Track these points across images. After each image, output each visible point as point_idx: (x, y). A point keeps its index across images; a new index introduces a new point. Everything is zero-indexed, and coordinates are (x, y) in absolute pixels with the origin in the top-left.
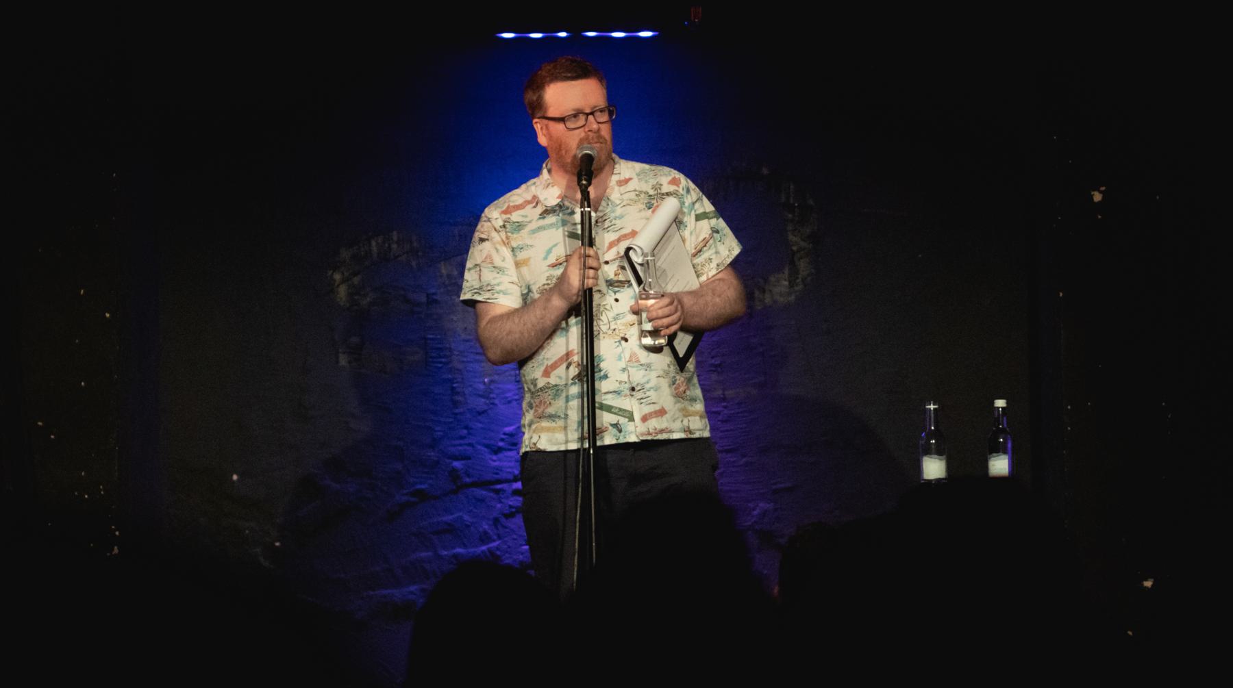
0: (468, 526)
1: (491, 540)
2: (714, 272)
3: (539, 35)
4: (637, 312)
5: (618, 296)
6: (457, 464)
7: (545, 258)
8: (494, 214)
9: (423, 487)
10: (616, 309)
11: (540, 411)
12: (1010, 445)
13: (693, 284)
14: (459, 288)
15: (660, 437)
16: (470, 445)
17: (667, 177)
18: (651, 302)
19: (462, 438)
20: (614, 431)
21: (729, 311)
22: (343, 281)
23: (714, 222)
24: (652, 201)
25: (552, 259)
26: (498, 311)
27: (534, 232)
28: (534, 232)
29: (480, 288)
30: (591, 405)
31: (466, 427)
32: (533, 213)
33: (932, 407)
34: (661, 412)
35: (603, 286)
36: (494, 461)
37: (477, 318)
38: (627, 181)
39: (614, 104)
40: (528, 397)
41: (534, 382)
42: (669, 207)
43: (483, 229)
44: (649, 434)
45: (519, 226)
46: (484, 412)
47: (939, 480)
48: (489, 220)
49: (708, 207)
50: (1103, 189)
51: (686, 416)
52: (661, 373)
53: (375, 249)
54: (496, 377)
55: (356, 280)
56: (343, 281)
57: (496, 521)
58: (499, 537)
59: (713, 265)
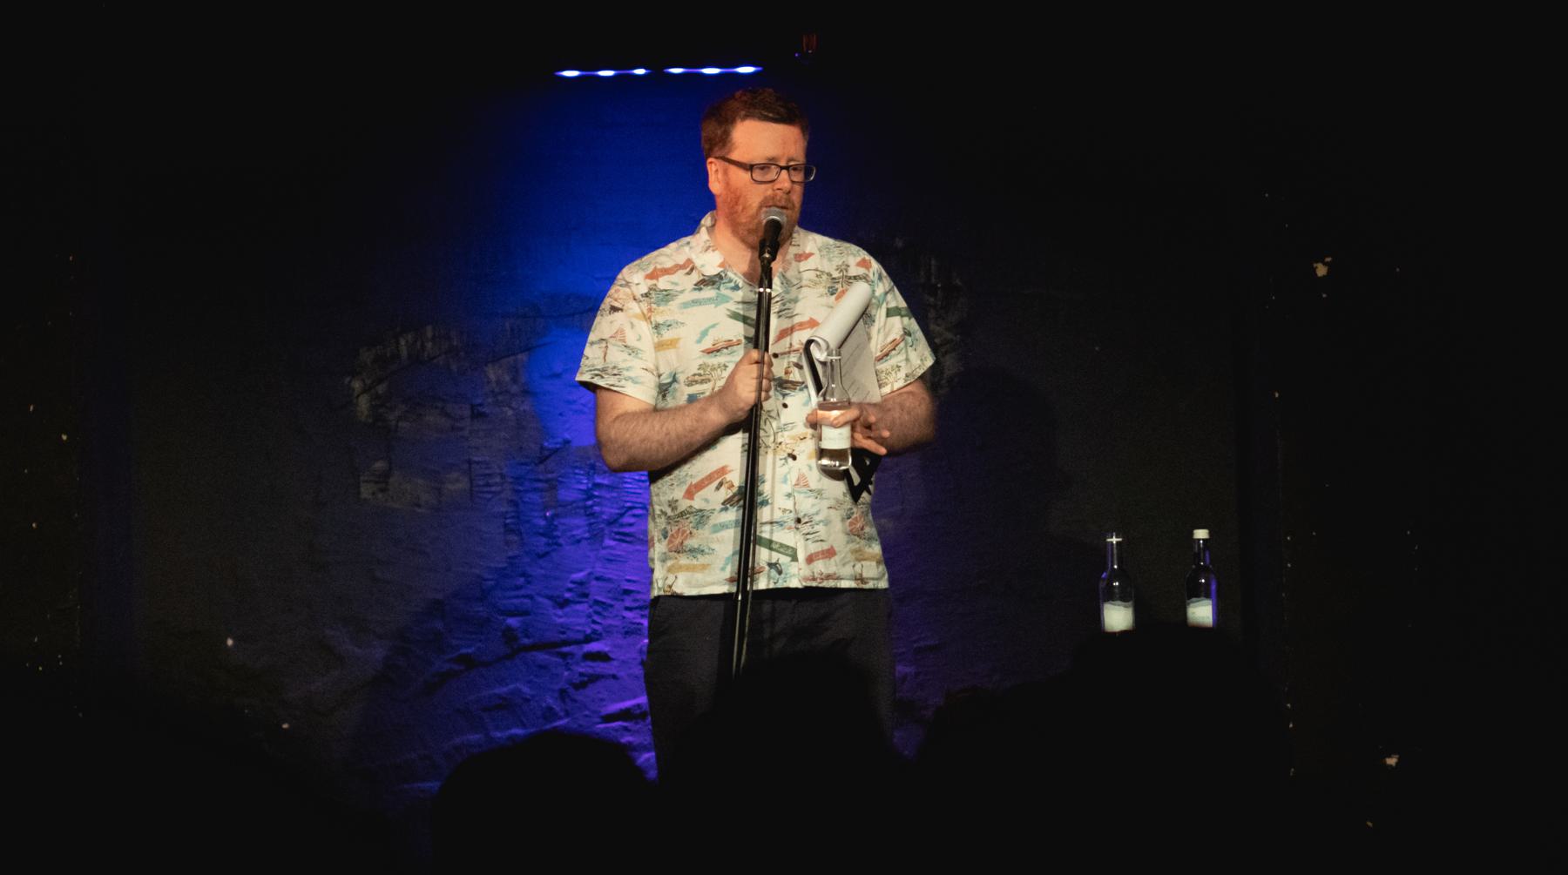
0: (527, 700)
1: (557, 717)
2: (901, 383)
3: (610, 73)
4: (814, 425)
5: (788, 401)
6: (513, 622)
7: (699, 341)
8: (634, 277)
10: (793, 412)
11: (677, 541)
12: (1214, 587)
14: (576, 366)
17: (854, 257)
18: (835, 413)
19: (518, 588)
22: (364, 391)
23: (906, 320)
24: (837, 286)
25: (708, 343)
26: (629, 406)
27: (685, 305)
28: (685, 305)
29: (603, 370)
30: (749, 538)
31: (524, 574)
32: (686, 282)
33: (1114, 540)
34: (830, 553)
36: (560, 617)
37: (594, 412)
42: (857, 295)
43: (617, 294)
45: (667, 296)
46: (547, 553)
47: (1123, 633)
48: (627, 284)
51: (859, 560)
52: (832, 503)
53: (404, 352)
55: (381, 389)
56: (364, 391)
57: (563, 694)
58: (567, 714)
59: (902, 375)
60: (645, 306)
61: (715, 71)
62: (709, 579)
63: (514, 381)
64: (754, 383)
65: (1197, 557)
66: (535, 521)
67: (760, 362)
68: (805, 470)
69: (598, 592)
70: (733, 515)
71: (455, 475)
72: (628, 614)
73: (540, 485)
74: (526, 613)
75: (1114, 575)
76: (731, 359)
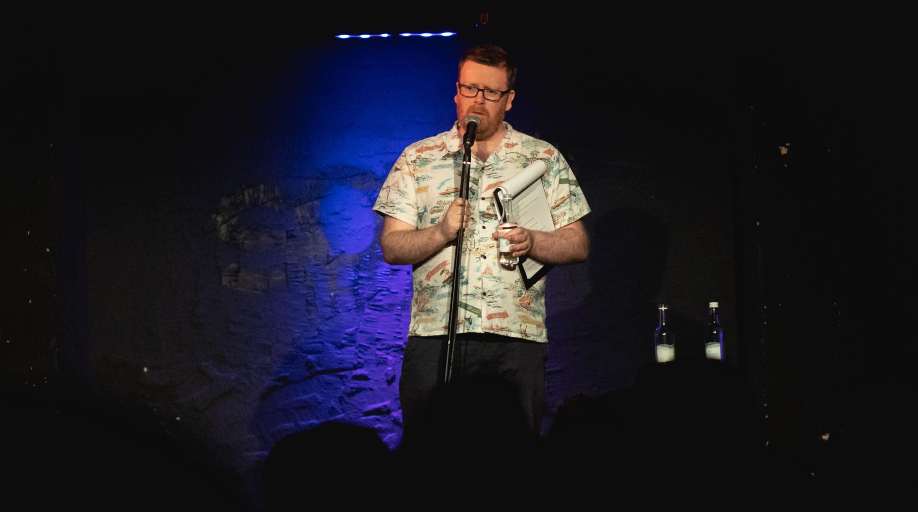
2: (566, 223)
3: (367, 36)
5: (486, 225)
7: (439, 188)
8: (411, 152)
9: (286, 374)
12: (721, 336)
13: (551, 228)
15: (500, 333)
16: (320, 342)
20: (467, 323)
21: (571, 252)
22: (224, 222)
23: (573, 188)
25: (443, 190)
26: (398, 227)
27: (435, 168)
28: (435, 168)
29: (386, 204)
30: (455, 304)
31: (318, 330)
32: (438, 154)
33: (663, 308)
34: (504, 315)
35: (476, 216)
36: (338, 354)
38: (513, 145)
39: (515, 84)
40: (415, 294)
41: (420, 283)
42: (537, 167)
43: (401, 160)
44: (492, 329)
46: (331, 318)
49: (572, 177)
50: (788, 144)
53: (247, 197)
54: (338, 292)
55: (234, 221)
56: (224, 222)
57: (341, 399)
58: (344, 411)
59: (566, 218)
60: (412, 167)
61: (429, 35)
62: (434, 327)
63: (312, 216)
64: (459, 217)
65: (712, 318)
66: (325, 298)
67: (463, 205)
68: (491, 265)
69: (361, 340)
70: (447, 290)
71: (277, 272)
72: (378, 352)
73: (326, 277)
74: (320, 352)
75: (663, 329)
76: (451, 198)
